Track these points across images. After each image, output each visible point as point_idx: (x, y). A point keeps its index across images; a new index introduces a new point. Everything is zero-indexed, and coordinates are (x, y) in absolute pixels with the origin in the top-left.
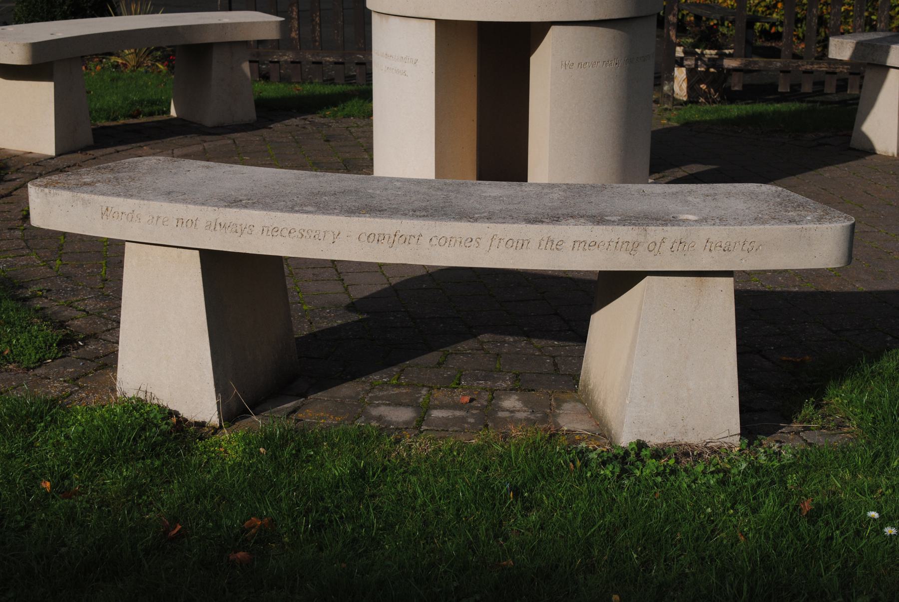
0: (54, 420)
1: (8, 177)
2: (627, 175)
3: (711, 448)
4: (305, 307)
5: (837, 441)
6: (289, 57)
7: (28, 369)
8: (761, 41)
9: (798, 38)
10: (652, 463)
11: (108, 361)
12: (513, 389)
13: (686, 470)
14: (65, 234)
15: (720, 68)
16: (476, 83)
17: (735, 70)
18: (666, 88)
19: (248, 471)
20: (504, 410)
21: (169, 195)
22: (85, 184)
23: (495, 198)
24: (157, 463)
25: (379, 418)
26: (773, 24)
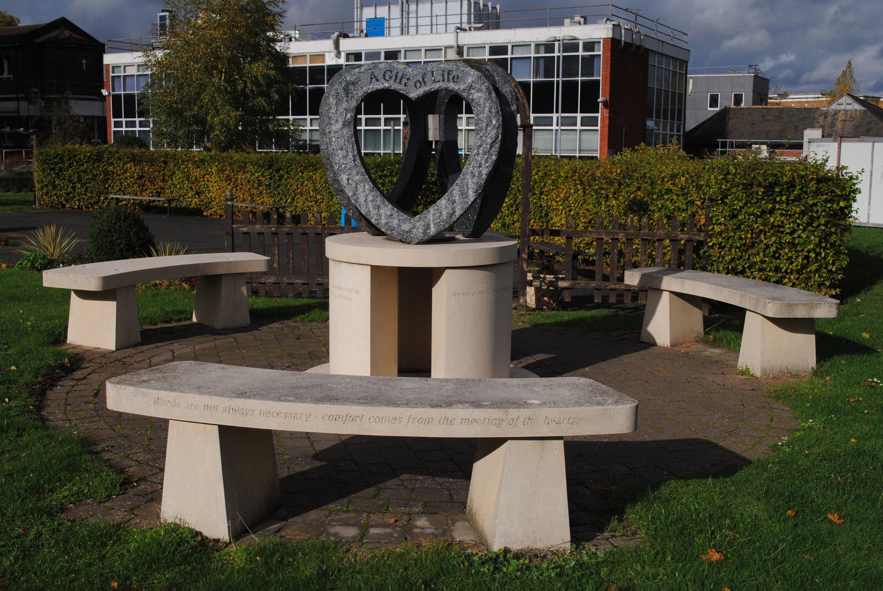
0: (119, 539)
1: (84, 366)
2: (496, 372)
3: (552, 551)
4: (285, 457)
5: (632, 544)
6: (272, 280)
7: (100, 502)
8: (583, 267)
9: (607, 264)
10: (514, 562)
11: (155, 497)
13: (536, 567)
15: (556, 287)
16: (397, 302)
17: (566, 288)
18: (521, 301)
19: (249, 573)
20: (417, 527)
21: (199, 389)
22: (144, 381)
23: (410, 389)
24: (189, 568)
25: (335, 535)
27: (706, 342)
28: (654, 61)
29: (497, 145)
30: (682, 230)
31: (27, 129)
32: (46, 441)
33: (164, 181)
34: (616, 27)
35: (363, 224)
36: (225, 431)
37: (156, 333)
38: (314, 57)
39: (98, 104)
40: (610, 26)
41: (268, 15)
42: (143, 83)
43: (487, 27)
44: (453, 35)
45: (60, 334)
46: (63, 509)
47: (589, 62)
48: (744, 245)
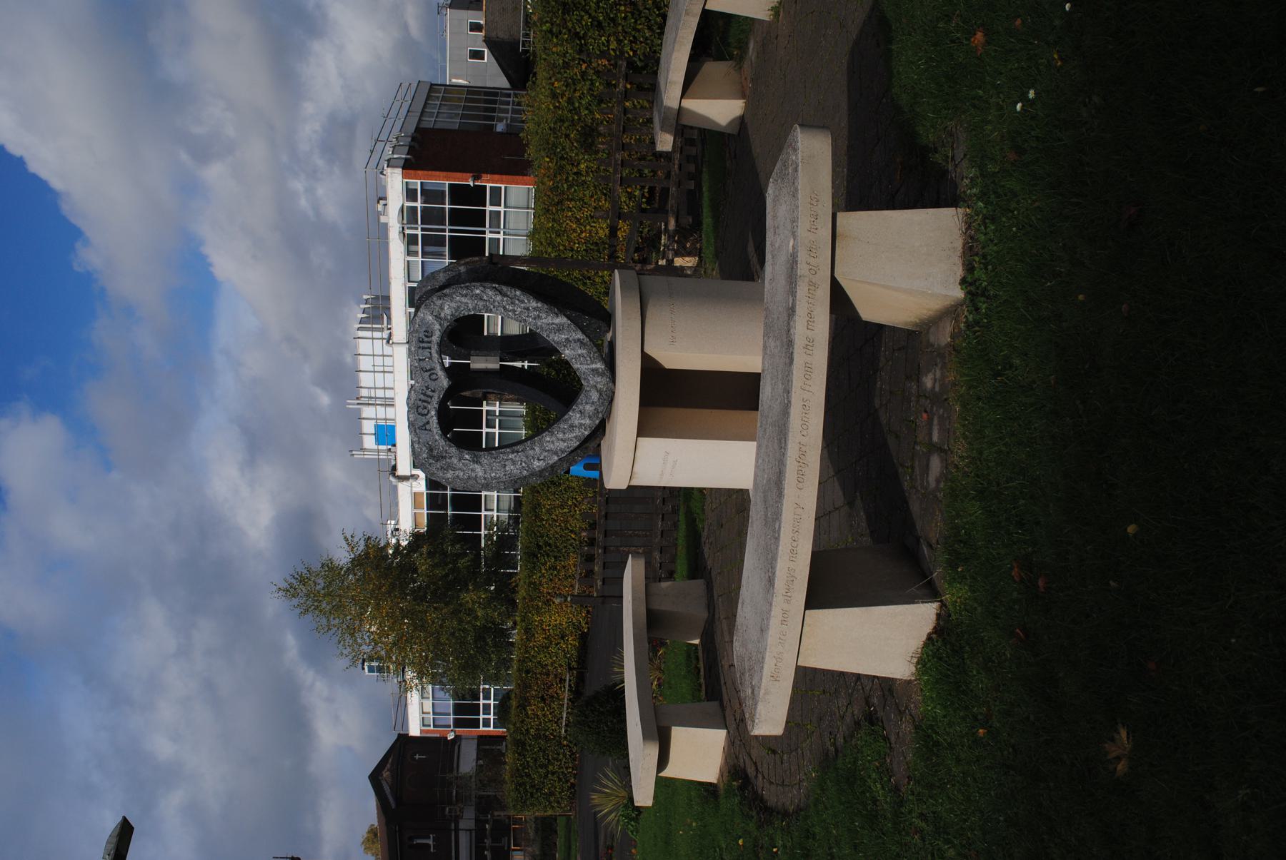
0: (931, 727)
2: (758, 298)
6: (657, 555)
7: (891, 748)
8: (655, 202)
11: (886, 685)
12: (918, 380)
14: (787, 722)
17: (677, 221)
20: (934, 387)
21: (763, 630)
25: (938, 481)
26: (643, 196)
27: (740, 60)
28: (429, 122)
29: (504, 288)
30: (615, 86)
31: (487, 821)
32: (821, 807)
33: (548, 674)
34: (390, 163)
35: (592, 445)
36: (813, 601)
37: (706, 683)
38: (416, 504)
39: (463, 743)
40: (388, 171)
41: (367, 554)
42: (441, 694)
43: (387, 309)
44: (396, 348)
45: (706, 790)
46: (896, 789)
47: (429, 195)
48: (633, 14)
